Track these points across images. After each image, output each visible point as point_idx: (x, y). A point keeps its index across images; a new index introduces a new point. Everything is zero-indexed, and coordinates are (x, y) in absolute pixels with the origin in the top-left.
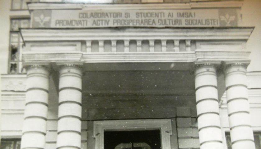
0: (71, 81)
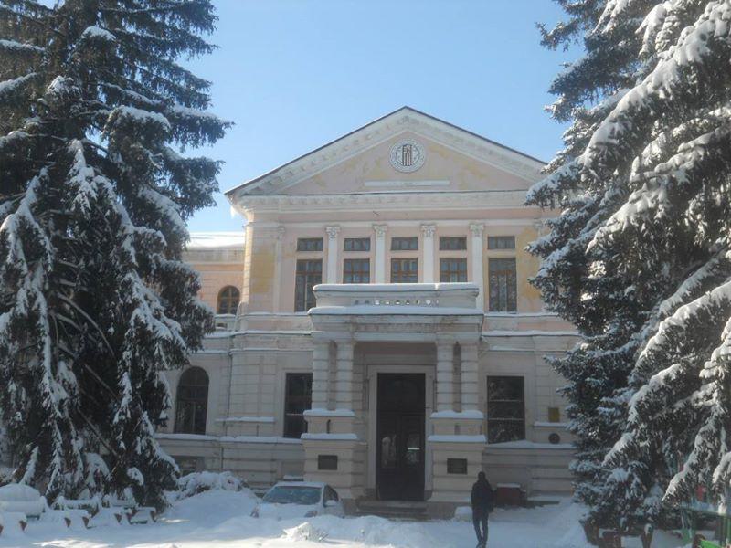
0: (346, 353)
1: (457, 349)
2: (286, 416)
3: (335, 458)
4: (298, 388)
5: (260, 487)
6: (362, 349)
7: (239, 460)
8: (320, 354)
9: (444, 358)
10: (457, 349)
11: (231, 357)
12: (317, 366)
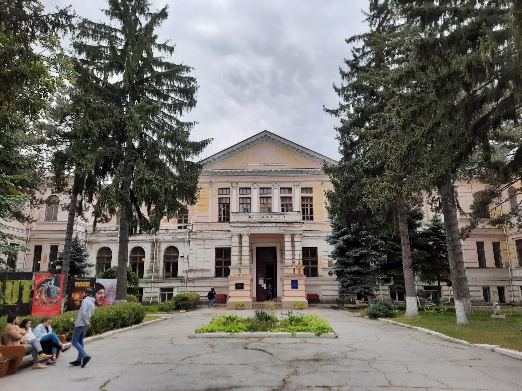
0: (246, 240)
1: (293, 236)
2: (215, 268)
3: (243, 284)
4: (223, 255)
5: (196, 284)
6: (252, 237)
7: (195, 287)
8: (237, 239)
10: (293, 236)
11: (189, 241)
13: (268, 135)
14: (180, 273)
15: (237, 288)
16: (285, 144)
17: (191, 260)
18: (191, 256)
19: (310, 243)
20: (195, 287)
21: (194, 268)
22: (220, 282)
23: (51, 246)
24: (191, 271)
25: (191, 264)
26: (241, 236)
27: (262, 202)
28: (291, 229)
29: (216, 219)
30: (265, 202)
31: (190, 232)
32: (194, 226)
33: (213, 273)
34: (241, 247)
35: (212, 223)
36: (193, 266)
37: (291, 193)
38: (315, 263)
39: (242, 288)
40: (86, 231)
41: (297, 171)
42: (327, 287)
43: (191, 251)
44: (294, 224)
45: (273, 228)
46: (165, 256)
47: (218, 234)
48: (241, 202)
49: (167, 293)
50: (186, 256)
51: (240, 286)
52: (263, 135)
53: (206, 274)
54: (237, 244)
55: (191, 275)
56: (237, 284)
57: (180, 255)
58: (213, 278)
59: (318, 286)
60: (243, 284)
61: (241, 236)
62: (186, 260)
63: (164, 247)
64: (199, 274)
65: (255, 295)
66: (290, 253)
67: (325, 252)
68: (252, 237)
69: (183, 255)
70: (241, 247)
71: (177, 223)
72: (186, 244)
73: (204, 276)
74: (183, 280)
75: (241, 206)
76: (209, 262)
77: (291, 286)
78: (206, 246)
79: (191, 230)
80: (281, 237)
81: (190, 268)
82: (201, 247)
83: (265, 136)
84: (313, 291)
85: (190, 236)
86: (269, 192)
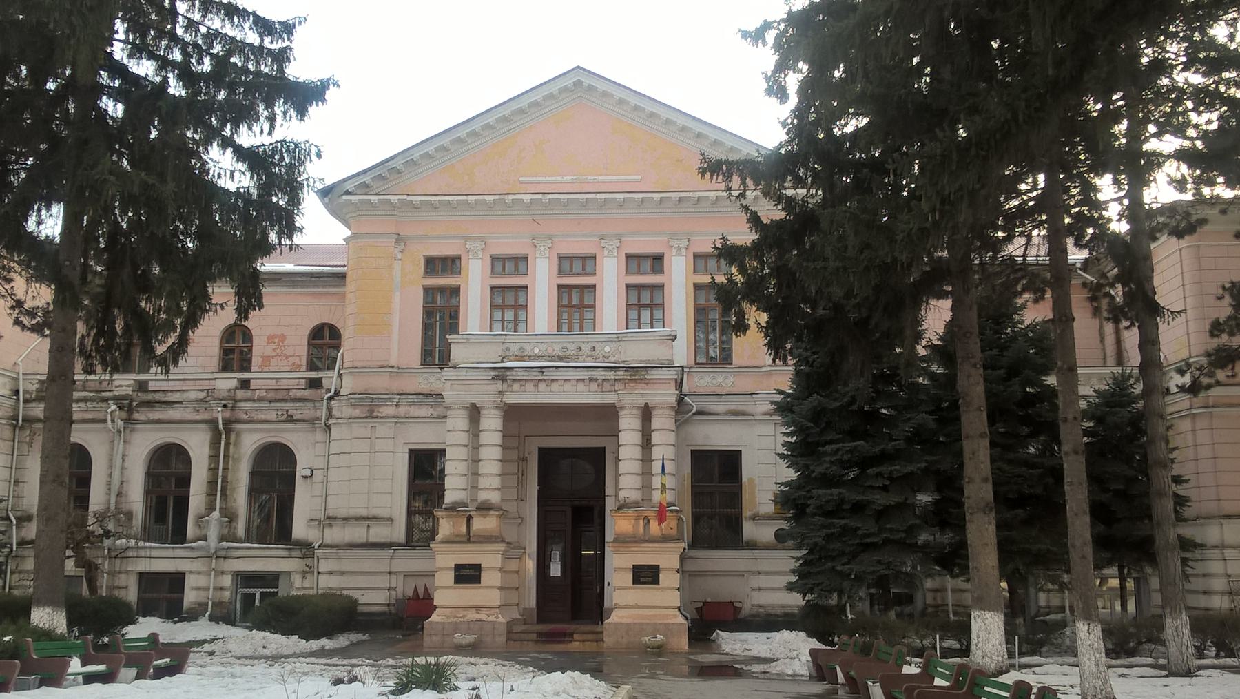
0: (492, 422)
3: (477, 568)
6: (513, 414)
8: (459, 421)
9: (629, 426)
12: (451, 437)
13: (587, 81)
14: (299, 530)
15: (458, 580)
16: (643, 110)
17: (333, 487)
18: (333, 475)
19: (718, 437)
20: (342, 573)
21: (343, 513)
22: (411, 562)
23: (411, 451)
24: (330, 520)
25: (332, 502)
26: (474, 412)
27: (565, 302)
28: (640, 388)
29: (414, 355)
30: (575, 302)
31: (331, 398)
32: (344, 378)
33: (399, 533)
34: (475, 446)
35: (401, 370)
36: (338, 506)
37: (662, 272)
38: (735, 498)
39: (655, 580)
40: (17, 392)
41: (680, 200)
42: (372, 578)
43: (334, 461)
44: (654, 372)
45: (581, 386)
46: (253, 474)
47: (421, 405)
48: (499, 301)
49: (257, 592)
50: (318, 476)
51: (471, 572)
52: (569, 82)
53: (379, 533)
54: (463, 438)
55: (334, 535)
56: (458, 568)
57: (301, 471)
58: (400, 545)
59: (741, 575)
60: (477, 568)
61: (474, 412)
62: (318, 489)
63: (250, 441)
64: (357, 533)
65: (531, 601)
66: (636, 438)
67: (767, 467)
68: (513, 414)
69: (308, 473)
70: (475, 446)
71: (304, 368)
72: (320, 436)
73: (372, 539)
74: (306, 548)
75: (498, 315)
76: (391, 494)
77: (452, 574)
78: (380, 445)
79: (337, 393)
80: (608, 414)
81: (331, 513)
82: (364, 446)
83: (578, 83)
84: (723, 590)
85: (329, 410)
86: (588, 268)
